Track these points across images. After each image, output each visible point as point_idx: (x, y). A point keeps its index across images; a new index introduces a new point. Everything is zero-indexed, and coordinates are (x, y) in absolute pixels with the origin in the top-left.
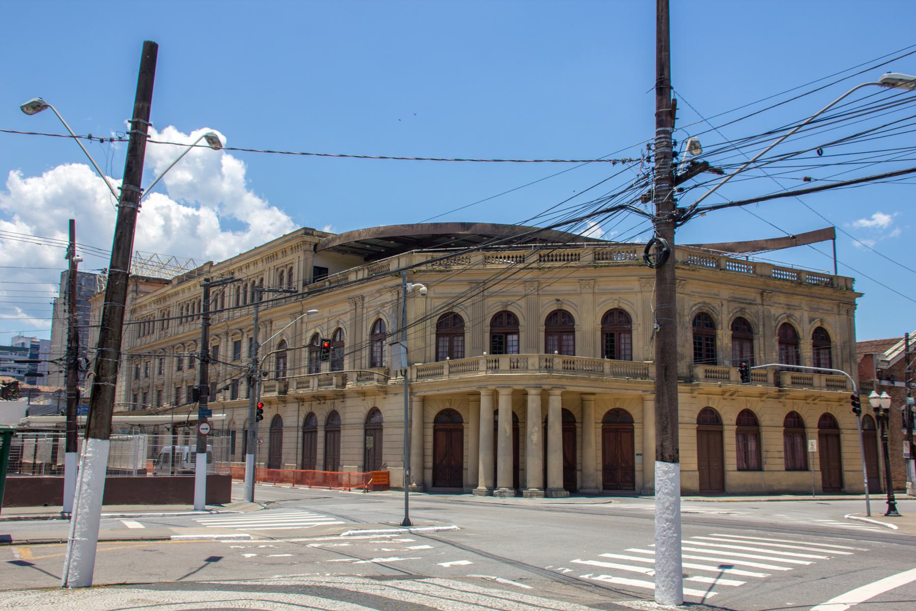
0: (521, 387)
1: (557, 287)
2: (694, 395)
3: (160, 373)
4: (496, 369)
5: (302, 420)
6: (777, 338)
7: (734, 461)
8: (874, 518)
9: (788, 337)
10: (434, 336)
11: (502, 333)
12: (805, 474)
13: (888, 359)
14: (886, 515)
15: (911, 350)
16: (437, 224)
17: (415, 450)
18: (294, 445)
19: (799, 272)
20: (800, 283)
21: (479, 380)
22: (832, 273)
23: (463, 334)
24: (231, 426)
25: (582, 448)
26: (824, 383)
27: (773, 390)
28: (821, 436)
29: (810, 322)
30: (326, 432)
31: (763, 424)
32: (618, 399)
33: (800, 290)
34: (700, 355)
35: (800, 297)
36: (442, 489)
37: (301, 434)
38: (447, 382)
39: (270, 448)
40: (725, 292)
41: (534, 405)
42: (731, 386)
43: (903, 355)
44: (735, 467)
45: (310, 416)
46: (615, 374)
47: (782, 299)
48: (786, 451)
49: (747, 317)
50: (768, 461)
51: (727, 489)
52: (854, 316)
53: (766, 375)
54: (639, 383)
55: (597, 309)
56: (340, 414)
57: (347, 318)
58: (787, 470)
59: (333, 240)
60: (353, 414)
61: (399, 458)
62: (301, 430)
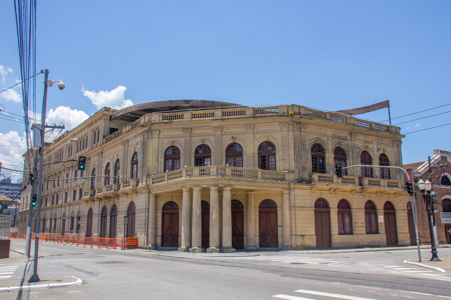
0: (206, 186)
1: (232, 130)
2: (313, 191)
3: (47, 189)
4: (191, 175)
5: (101, 210)
6: (360, 159)
7: (337, 229)
8: (424, 262)
9: (366, 158)
10: (163, 160)
11: (202, 156)
12: (377, 235)
13: (420, 171)
14: (430, 260)
15: (432, 165)
16: (171, 101)
17: (151, 225)
18: (97, 224)
19: (300, 107)
20: (372, 129)
21: (182, 182)
22: (388, 124)
23: (179, 158)
24: (79, 214)
25: (247, 223)
26: (386, 184)
27: (358, 188)
28: (385, 214)
29: (378, 151)
30: (111, 216)
31: (353, 207)
32: (268, 194)
33: (371, 132)
34: (316, 168)
35: (372, 137)
36: (166, 248)
37: (100, 217)
38: (167, 185)
39: (87, 226)
40: (330, 132)
41: (214, 197)
42: (334, 186)
43: (428, 169)
44: (337, 233)
45: (104, 208)
46: (265, 179)
47: (362, 137)
48: (366, 223)
49: (342, 147)
50: (356, 228)
51: (333, 245)
52: (401, 148)
53: (354, 179)
54: (279, 183)
55: (256, 142)
56: (117, 206)
57: (121, 153)
58: (367, 233)
59: (119, 112)
60: (122, 206)
61: (143, 230)
62: (100, 216)
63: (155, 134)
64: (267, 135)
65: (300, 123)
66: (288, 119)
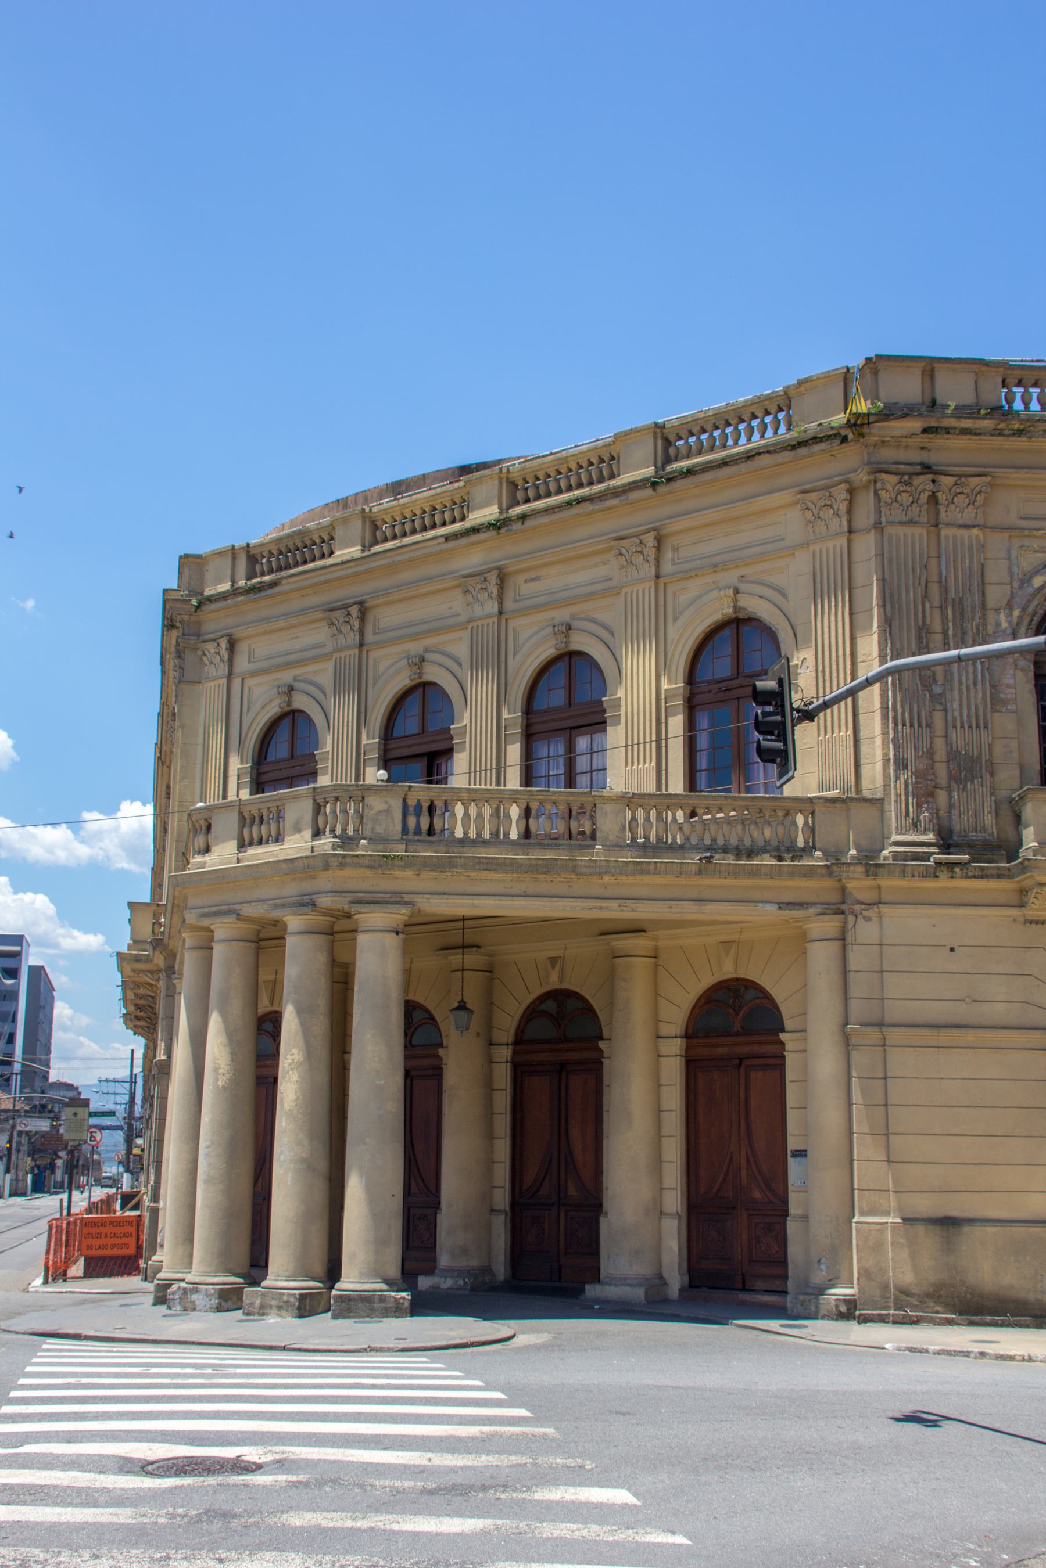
1: (557, 579)
19: (930, 367)
32: (727, 945)
55: (673, 631)
63: (215, 653)
64: (731, 577)
65: (927, 468)
66: (849, 459)
